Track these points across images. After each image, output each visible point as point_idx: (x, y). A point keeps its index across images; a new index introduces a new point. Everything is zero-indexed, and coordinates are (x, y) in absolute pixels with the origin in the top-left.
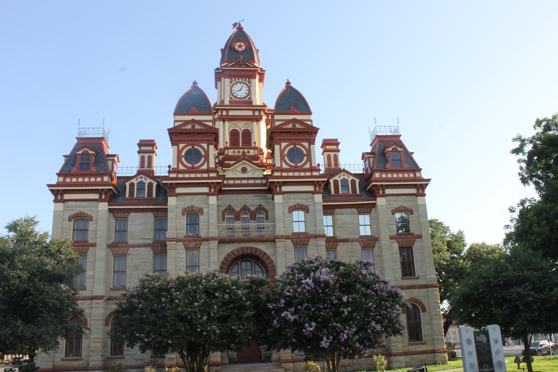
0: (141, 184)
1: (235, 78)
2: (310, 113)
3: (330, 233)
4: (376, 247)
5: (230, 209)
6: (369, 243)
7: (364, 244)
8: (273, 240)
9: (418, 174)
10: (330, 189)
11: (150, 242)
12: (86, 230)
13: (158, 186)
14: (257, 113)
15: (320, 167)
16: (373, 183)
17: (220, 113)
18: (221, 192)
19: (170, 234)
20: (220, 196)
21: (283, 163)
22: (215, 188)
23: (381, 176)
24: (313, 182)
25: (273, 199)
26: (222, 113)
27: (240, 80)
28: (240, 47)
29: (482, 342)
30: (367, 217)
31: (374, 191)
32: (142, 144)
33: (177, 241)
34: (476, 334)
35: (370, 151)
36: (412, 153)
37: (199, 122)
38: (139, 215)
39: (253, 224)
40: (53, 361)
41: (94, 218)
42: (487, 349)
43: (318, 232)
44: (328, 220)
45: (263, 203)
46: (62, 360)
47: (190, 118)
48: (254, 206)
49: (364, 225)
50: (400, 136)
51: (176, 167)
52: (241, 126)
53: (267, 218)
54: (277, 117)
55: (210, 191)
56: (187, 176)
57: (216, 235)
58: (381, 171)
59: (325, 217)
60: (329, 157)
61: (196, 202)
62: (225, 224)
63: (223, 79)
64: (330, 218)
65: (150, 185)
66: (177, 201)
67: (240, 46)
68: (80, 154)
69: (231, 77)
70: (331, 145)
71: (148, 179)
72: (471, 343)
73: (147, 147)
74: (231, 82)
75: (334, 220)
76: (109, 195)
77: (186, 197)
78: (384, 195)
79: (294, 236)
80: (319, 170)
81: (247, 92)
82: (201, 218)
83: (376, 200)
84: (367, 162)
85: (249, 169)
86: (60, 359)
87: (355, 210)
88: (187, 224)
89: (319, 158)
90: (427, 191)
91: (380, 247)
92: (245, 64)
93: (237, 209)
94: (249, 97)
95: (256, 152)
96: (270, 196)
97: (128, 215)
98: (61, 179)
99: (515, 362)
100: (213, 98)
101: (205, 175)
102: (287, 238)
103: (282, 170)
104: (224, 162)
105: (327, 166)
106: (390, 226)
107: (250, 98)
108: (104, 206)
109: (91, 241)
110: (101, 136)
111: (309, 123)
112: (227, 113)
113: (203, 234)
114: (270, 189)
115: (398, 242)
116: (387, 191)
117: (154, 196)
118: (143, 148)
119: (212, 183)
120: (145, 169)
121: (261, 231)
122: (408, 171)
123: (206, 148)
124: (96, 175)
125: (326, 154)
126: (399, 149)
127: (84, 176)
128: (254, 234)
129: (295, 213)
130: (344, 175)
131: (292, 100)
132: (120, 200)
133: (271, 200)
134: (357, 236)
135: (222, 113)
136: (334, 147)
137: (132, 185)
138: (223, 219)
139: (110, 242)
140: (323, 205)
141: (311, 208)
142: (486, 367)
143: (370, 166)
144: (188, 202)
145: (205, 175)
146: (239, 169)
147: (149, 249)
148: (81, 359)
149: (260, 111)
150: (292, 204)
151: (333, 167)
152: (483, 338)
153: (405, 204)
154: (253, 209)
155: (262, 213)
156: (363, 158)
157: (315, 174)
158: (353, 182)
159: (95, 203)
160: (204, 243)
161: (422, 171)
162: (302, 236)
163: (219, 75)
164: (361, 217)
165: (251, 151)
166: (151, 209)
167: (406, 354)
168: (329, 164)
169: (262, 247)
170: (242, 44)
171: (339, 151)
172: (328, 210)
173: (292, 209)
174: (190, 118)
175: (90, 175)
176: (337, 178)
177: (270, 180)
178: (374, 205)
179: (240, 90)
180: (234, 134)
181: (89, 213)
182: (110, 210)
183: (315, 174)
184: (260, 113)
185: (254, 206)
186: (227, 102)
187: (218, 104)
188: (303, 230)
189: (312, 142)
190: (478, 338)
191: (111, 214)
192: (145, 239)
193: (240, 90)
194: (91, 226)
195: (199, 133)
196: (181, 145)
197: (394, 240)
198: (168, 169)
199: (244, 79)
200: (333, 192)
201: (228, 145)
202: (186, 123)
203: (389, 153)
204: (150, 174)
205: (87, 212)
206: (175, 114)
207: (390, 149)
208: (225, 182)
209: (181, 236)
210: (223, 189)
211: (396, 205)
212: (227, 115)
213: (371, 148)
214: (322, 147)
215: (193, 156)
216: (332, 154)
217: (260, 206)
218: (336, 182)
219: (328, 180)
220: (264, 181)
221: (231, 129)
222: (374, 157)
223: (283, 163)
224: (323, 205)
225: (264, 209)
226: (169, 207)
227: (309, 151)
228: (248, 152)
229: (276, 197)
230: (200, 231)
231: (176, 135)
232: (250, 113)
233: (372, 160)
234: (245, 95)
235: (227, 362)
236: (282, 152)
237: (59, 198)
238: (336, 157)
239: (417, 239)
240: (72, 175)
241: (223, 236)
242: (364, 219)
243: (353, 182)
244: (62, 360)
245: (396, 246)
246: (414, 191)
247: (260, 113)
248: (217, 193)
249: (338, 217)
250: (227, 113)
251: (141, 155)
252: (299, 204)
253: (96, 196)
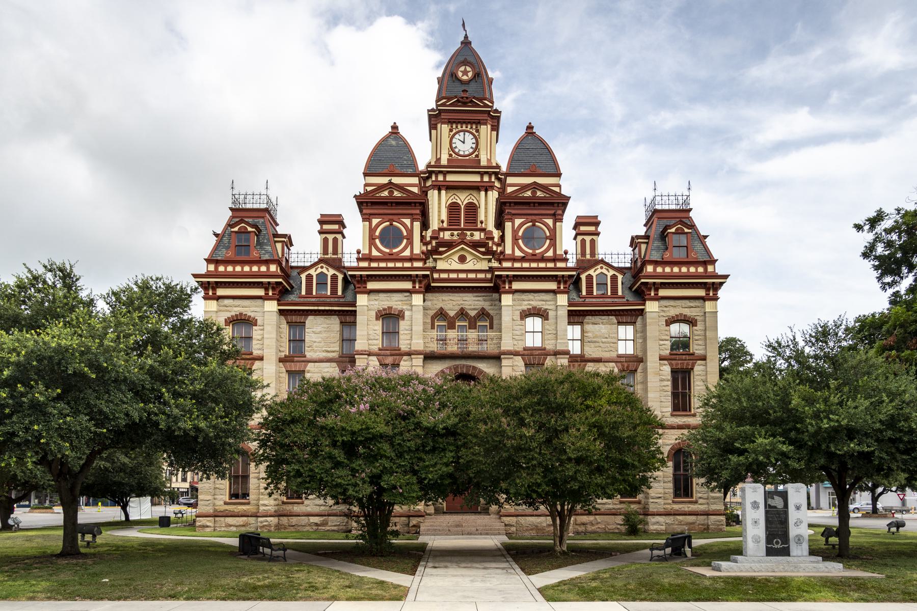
0: (322, 276)
1: (457, 123)
2: (559, 175)
3: (575, 348)
4: (639, 370)
5: (441, 314)
6: (633, 364)
7: (623, 366)
8: (496, 358)
9: (710, 268)
10: (583, 293)
11: (335, 355)
12: (250, 338)
13: (346, 281)
14: (486, 179)
15: (568, 256)
16: (643, 281)
17: (434, 178)
18: (428, 289)
19: (360, 345)
20: (429, 296)
21: (516, 249)
22: (420, 282)
23: (655, 269)
24: (556, 276)
25: (500, 301)
26: (437, 177)
27: (464, 128)
28: (465, 73)
29: (775, 507)
30: (630, 329)
31: (643, 292)
32: (324, 220)
33: (369, 355)
34: (768, 495)
35: (643, 234)
36: (706, 237)
37: (400, 187)
38: (320, 319)
39: (472, 335)
40: (214, 505)
41: (259, 322)
42: (783, 516)
43: (560, 348)
44: (574, 331)
45: (486, 305)
46: (226, 503)
47: (384, 180)
48: (474, 309)
49: (624, 341)
50: (690, 210)
51: (367, 252)
52: (463, 199)
53: (491, 327)
54: (510, 180)
55: (414, 287)
56: (383, 265)
57: (421, 348)
58: (656, 263)
59: (570, 328)
60: (583, 242)
61: (395, 302)
62: (434, 333)
63: (439, 125)
64: (578, 328)
65: (334, 278)
66: (369, 300)
67: (465, 73)
68: (236, 232)
69: (450, 122)
70: (588, 226)
71: (330, 269)
72: (758, 507)
73: (332, 225)
74: (451, 130)
75: (583, 331)
76: (278, 290)
77: (382, 295)
78: (657, 298)
79: (526, 352)
80: (566, 260)
81: (474, 146)
82: (401, 323)
83: (644, 304)
84: (637, 251)
85: (469, 258)
86: (222, 503)
87: (613, 319)
88: (383, 333)
89: (568, 242)
90: (720, 293)
91: (645, 370)
92: (471, 101)
93: (452, 313)
94: (476, 153)
95: (482, 234)
96: (496, 295)
97: (306, 319)
98: (212, 267)
99: (822, 535)
100: (423, 157)
101: (407, 265)
102: (516, 354)
103: (514, 259)
104: (437, 248)
105: (579, 256)
106: (662, 342)
107: (477, 156)
108: (272, 306)
109: (256, 353)
110: (264, 206)
111: (557, 189)
112: (445, 177)
113: (404, 347)
114: (496, 286)
115: (670, 364)
116: (662, 293)
117: (340, 293)
118: (326, 227)
119: (417, 275)
120: (329, 256)
121: (481, 344)
122: (696, 263)
123: (409, 225)
124: (259, 262)
125: (580, 238)
126: (686, 230)
127: (243, 263)
128: (472, 348)
129: (529, 320)
130: (602, 268)
131: (535, 153)
132: (292, 298)
133: (497, 302)
134: (613, 355)
135: (437, 177)
136: (592, 228)
137: (309, 277)
138: (433, 327)
139: (282, 355)
140: (569, 311)
141: (551, 314)
142: (777, 543)
143: (640, 256)
144: (383, 302)
145: (407, 265)
146: (456, 258)
147: (334, 364)
148: (248, 504)
149: (490, 174)
150: (525, 308)
151: (588, 257)
152: (778, 502)
153: (687, 312)
154: (473, 313)
155: (486, 319)
156: (631, 245)
157: (560, 265)
158: (614, 278)
159: (259, 302)
160: (405, 358)
161: (717, 264)
162: (537, 352)
163: (435, 119)
164: (621, 328)
165: (475, 233)
166: (335, 311)
167: (667, 514)
168: (583, 253)
169: (483, 366)
170: (468, 69)
171: (598, 234)
172: (575, 316)
173: (525, 315)
174: (384, 180)
175: (251, 263)
176: (591, 272)
177: (496, 273)
178: (642, 312)
179: (464, 144)
180: (453, 208)
181: (252, 315)
182: (281, 312)
183: (560, 265)
184: (490, 178)
185: (474, 309)
186: (444, 162)
187: (433, 163)
188: (538, 344)
189: (558, 218)
190: (770, 502)
191: (282, 317)
192: (328, 352)
193: (464, 144)
194: (256, 332)
195: (399, 203)
196: (375, 221)
197: (666, 362)
198: (356, 256)
199: (469, 126)
200: (584, 293)
201: (445, 225)
202: (381, 187)
203: (671, 228)
204: (336, 264)
205: (249, 314)
206: (366, 175)
207: (673, 230)
208: (436, 276)
209: (375, 349)
210: (433, 285)
211: (673, 312)
212: (445, 181)
213: (645, 229)
214: (575, 228)
215: (391, 237)
216: (588, 239)
217: (483, 309)
218: (590, 278)
219: (579, 275)
220: (489, 276)
221: (450, 201)
222: (647, 243)
223: (516, 249)
224: (569, 311)
225: (488, 315)
226: (358, 309)
227: (553, 231)
228: (472, 235)
229: (504, 297)
230: (401, 342)
231: (368, 203)
232: (477, 178)
233: (643, 247)
234: (471, 150)
235: (433, 511)
236: (515, 232)
237: (211, 293)
238: (593, 243)
239: (699, 362)
240: (226, 262)
241: (431, 349)
242: (627, 331)
243: (614, 278)
244: (226, 503)
245: (667, 369)
246: (701, 293)
247: (490, 178)
248: (423, 289)
249: (588, 327)
250: (445, 177)
251: (324, 236)
252: (534, 308)
253: (260, 292)
